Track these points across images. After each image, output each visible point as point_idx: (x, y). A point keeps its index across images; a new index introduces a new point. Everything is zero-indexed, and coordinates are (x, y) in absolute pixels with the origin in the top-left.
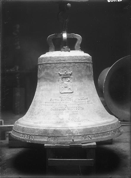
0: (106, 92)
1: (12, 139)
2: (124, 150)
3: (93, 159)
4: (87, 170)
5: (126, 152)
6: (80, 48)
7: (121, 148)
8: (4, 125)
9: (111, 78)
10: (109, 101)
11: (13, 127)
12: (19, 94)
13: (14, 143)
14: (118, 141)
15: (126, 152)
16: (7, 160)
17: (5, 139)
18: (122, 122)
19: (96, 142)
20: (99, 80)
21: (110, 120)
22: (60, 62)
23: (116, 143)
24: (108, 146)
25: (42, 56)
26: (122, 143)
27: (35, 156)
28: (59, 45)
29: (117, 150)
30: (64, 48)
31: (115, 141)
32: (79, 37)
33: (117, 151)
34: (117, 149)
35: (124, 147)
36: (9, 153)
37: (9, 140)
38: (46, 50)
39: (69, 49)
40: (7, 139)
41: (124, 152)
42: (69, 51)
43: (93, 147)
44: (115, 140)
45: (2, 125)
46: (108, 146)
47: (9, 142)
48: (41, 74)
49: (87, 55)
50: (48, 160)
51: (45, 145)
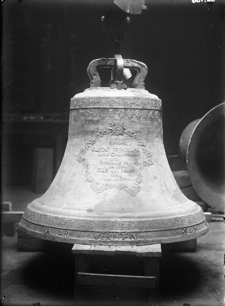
0: (190, 162)
1: (23, 235)
2: (215, 263)
3: (155, 277)
4: (145, 293)
5: (217, 266)
6: (143, 85)
7: (211, 260)
8: (13, 211)
9: (202, 137)
10: (196, 177)
11: (22, 215)
12: (32, 154)
13: (25, 242)
14: (208, 247)
15: (217, 266)
16: (12, 271)
17: (12, 235)
18: (214, 215)
19: (163, 246)
20: (181, 140)
21: (185, 208)
22: (102, 109)
23: (202, 251)
24: (189, 255)
25: (78, 96)
26: (213, 251)
27: (54, 263)
28: (110, 77)
29: (203, 263)
30: (117, 83)
31: (200, 247)
32: (143, 66)
33: (202, 265)
34: (202, 261)
35: (215, 258)
36: (13, 260)
37: (19, 237)
38: (85, 84)
39: (126, 86)
40: (16, 235)
41: (213, 267)
42: (126, 89)
43: (155, 256)
44: (202, 245)
45: (8, 211)
46: (189, 255)
47: (18, 241)
48: (73, 123)
49: (155, 97)
50: (77, 273)
51: (76, 247)
